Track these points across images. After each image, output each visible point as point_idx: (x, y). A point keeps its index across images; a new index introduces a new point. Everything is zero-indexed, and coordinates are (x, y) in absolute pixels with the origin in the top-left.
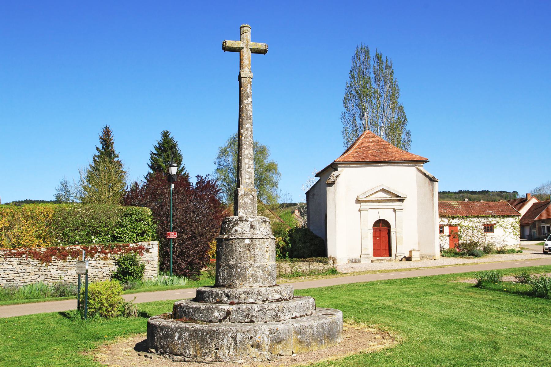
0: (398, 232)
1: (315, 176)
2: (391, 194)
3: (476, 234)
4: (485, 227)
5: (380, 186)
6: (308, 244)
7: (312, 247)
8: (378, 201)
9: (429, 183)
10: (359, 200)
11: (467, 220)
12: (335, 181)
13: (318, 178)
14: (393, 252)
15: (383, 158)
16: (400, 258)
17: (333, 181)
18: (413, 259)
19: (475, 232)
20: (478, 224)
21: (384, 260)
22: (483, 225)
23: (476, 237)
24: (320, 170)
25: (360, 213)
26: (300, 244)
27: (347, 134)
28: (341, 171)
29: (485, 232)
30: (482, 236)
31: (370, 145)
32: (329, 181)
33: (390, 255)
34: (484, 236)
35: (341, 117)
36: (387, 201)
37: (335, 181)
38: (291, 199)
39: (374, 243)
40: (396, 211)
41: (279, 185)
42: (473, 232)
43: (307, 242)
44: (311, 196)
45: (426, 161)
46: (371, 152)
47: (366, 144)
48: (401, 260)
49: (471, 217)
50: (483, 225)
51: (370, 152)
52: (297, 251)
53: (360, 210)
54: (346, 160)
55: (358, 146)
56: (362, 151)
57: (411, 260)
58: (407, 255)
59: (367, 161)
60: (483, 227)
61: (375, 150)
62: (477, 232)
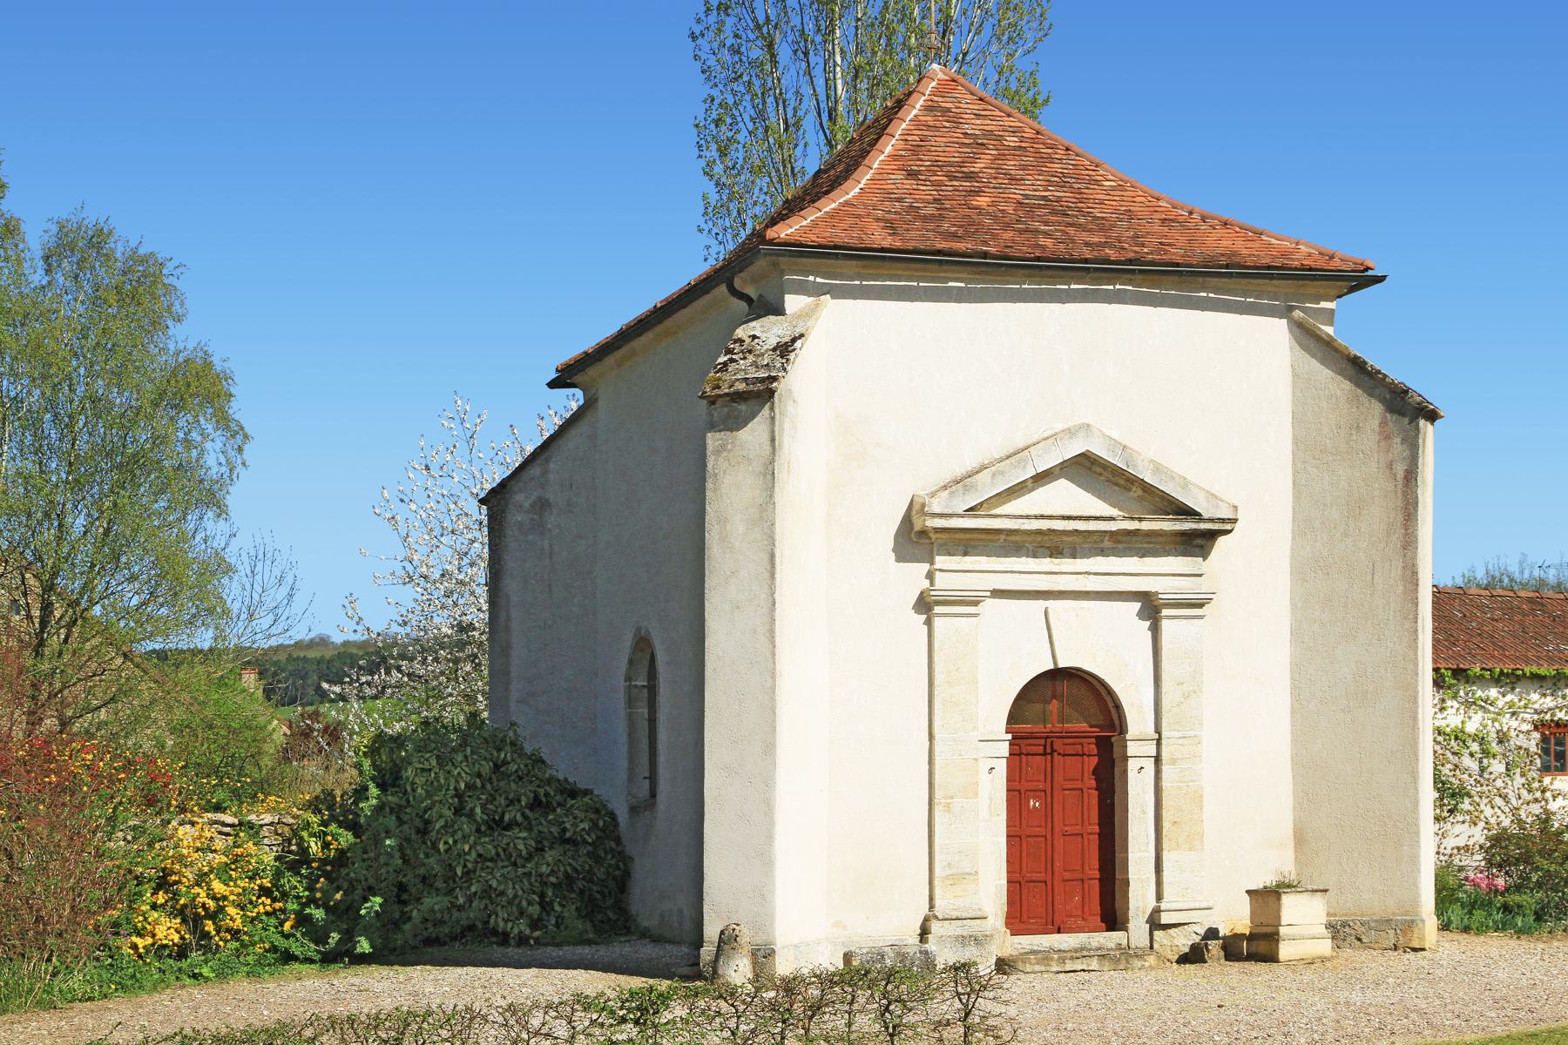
0: (1173, 761)
1: (553, 385)
2: (1137, 492)
3: (1499, 783)
4: (1544, 739)
5: (1070, 432)
6: (521, 841)
7: (550, 856)
8: (1051, 544)
9: (1383, 424)
10: (923, 533)
11: (1455, 697)
12: (775, 379)
13: (571, 400)
14: (1140, 898)
15: (1087, 244)
16: (1183, 941)
17: (762, 380)
18: (1285, 951)
19: (1498, 767)
20: (1514, 724)
21: (1081, 953)
22: (1536, 728)
23: (1499, 801)
24: (588, 341)
25: (929, 622)
26: (465, 838)
27: (723, 153)
28: (806, 314)
29: (1546, 769)
30: (1530, 797)
31: (974, 159)
32: (727, 377)
33: (1113, 919)
34: (1538, 794)
35: (697, 30)
36: (1107, 544)
37: (775, 379)
38: (289, 579)
39: (1015, 838)
40: (1165, 612)
41: (234, 499)
42: (1482, 770)
43: (512, 824)
44: (515, 517)
45: (1360, 279)
46: (993, 204)
47: (945, 146)
48: (1194, 956)
49: (1479, 680)
50: (1536, 728)
51: (982, 201)
52: (439, 884)
53: (925, 605)
54: (839, 235)
55: (894, 157)
56: (927, 192)
57: (1271, 958)
58: (1236, 918)
59: (985, 255)
60: (1533, 743)
61: (1016, 193)
62: (1502, 768)
